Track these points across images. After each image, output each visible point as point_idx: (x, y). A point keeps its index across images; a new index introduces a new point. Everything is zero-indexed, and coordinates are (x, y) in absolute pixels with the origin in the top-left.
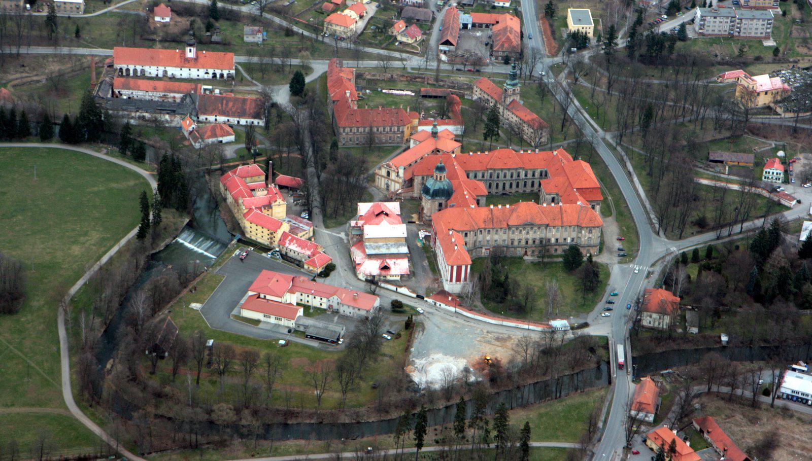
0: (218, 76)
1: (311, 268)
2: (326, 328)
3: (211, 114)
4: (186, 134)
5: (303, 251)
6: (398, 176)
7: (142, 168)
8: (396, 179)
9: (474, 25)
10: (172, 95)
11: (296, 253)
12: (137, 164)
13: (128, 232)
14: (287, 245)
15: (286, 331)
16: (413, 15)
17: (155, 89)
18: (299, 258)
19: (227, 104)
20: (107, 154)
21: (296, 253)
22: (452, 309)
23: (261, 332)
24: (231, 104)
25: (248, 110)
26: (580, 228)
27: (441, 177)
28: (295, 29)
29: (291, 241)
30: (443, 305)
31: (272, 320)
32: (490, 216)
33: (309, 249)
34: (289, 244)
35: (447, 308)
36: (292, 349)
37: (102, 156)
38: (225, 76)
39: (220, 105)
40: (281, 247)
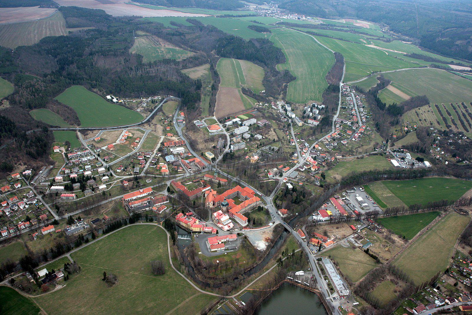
3: (157, 204)
15: (224, 250)
17: (139, 202)
20: (143, 223)
22: (249, 230)
28: (156, 176)
29: (205, 228)
30: (247, 230)
31: (219, 249)
37: (142, 224)
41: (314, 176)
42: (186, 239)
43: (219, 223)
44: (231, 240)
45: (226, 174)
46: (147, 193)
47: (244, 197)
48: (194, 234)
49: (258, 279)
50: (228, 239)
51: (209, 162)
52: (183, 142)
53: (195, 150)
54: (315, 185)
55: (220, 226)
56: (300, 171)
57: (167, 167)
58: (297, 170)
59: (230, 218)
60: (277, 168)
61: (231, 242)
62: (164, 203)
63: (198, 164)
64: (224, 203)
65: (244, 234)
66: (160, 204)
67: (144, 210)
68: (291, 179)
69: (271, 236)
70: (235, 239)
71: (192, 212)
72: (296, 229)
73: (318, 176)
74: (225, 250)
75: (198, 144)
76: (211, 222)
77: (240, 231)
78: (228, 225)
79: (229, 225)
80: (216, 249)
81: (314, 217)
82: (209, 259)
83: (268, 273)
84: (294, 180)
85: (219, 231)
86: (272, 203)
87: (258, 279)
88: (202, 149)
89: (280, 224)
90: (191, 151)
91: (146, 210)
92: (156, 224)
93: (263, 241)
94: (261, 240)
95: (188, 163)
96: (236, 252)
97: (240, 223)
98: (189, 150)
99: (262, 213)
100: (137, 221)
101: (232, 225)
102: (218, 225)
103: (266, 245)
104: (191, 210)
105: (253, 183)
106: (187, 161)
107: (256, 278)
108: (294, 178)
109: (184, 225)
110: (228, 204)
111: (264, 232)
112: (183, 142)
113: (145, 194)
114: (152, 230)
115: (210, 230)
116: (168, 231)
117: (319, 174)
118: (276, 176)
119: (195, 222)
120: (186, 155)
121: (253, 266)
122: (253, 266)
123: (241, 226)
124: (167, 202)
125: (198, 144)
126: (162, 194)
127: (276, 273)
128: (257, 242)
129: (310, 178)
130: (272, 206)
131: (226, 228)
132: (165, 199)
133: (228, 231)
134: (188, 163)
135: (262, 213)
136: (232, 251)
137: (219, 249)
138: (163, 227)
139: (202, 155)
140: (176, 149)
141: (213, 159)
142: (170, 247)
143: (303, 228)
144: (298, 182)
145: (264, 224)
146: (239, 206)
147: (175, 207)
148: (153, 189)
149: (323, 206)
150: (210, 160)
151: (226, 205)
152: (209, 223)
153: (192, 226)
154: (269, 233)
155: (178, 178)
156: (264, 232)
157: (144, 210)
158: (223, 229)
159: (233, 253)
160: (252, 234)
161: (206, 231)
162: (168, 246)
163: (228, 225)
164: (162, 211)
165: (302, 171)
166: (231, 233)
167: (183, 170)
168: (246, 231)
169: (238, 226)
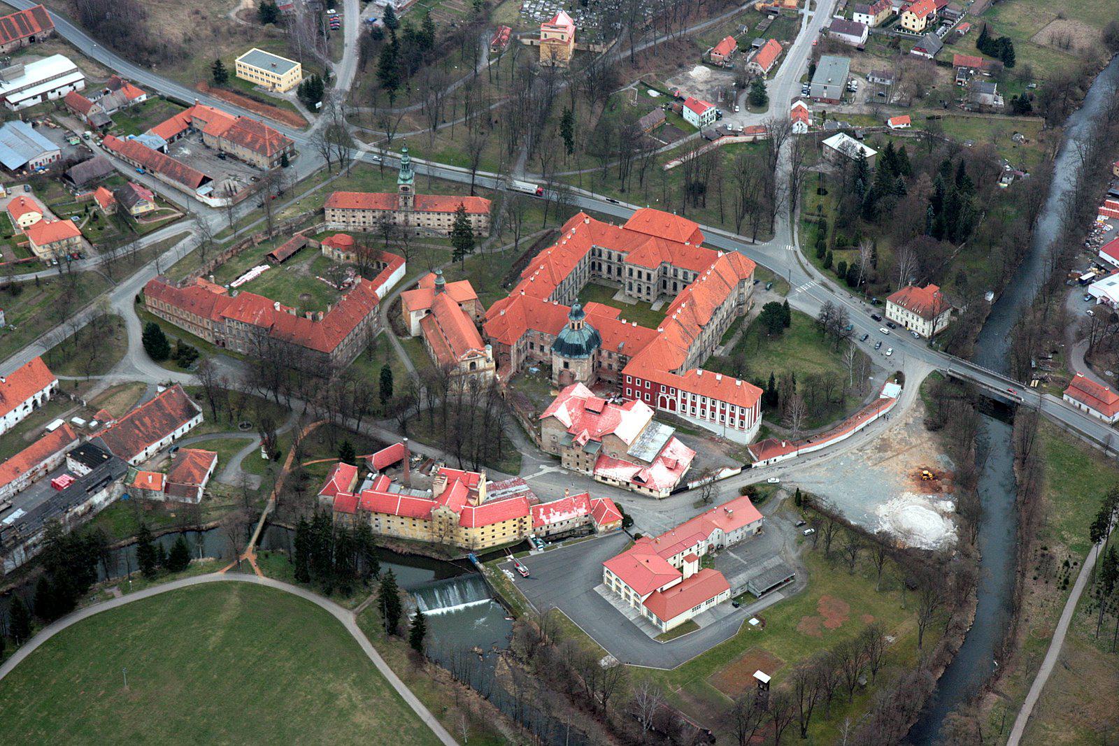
0: (39, 402)
1: (610, 525)
2: (767, 571)
3: (138, 452)
4: (161, 497)
5: (574, 514)
6: (488, 361)
7: (195, 575)
8: (487, 366)
9: (171, 140)
10: (42, 464)
11: (565, 523)
12: (182, 574)
13: (364, 654)
14: (546, 522)
15: (730, 609)
16: (89, 175)
17: (17, 472)
18: (569, 527)
19: (143, 424)
20: (125, 591)
21: (565, 523)
22: (794, 454)
23: (710, 633)
24: (147, 420)
25: (173, 413)
26: (88, 381)
27: (579, 324)
28: (19, 278)
29: (547, 512)
30: (779, 458)
31: (704, 607)
32: (682, 329)
33: (580, 507)
34: (548, 518)
35: (786, 457)
36: (778, 618)
37: (120, 600)
38: (48, 395)
39: (137, 431)
40: (538, 529)
41: (941, 58)
42: (461, 607)
43: (601, 459)
44: (734, 537)
45: (458, 173)
46: (30, 402)
47: (654, 275)
48: (498, 562)
49: (1027, 709)
50: (714, 539)
51: (290, 114)
52: (33, 21)
53: (145, 56)
54: (981, 109)
55: (623, 474)
56: (846, 49)
57: (43, 207)
58: (828, 45)
59: (660, 418)
60: (704, 63)
61: (735, 547)
62: (178, 433)
63: (235, 139)
64: (574, 338)
65: (777, 487)
66: (156, 445)
67: (80, 509)
68: (831, 110)
69: (937, 456)
70: (754, 527)
71: (397, 444)
72: (1042, 380)
73: (966, 54)
74: (736, 602)
75: (144, 16)
76: (546, 469)
77: (746, 474)
78: (665, 460)
79: (666, 454)
80: (688, 615)
81: (1093, 290)
82: (683, 683)
83: (1063, 663)
84: (846, 109)
85: (631, 507)
86: (811, 268)
87: (1027, 709)
88: (188, 40)
89: (934, 374)
90: (125, 70)
91: (91, 508)
92: (219, 576)
93: (907, 495)
94: (895, 493)
95: (161, 150)
96: (808, 599)
97: (716, 428)
98: (101, 65)
99: (796, 340)
100: (85, 591)
101: (682, 453)
102: (601, 472)
103: (944, 514)
104: (386, 435)
105: (633, 180)
106: (152, 139)
107: (1015, 708)
108: (843, 100)
109: (416, 532)
110: (595, 339)
111: (884, 446)
112: (33, 21)
113: (20, 408)
114: (223, 617)
115: (576, 516)
116: (328, 593)
117: (962, 43)
118: (732, 111)
119: (473, 494)
120: (113, 101)
121: (948, 647)
122: (948, 647)
123: (731, 443)
124: (193, 423)
125: (144, 16)
126: (124, 386)
127: (1101, 647)
128: (882, 510)
129: (931, 79)
130: (824, 285)
131: (663, 479)
132: (174, 409)
133: (679, 490)
134: (161, 150)
135: (796, 340)
136: (777, 597)
137: (704, 607)
138: (283, 578)
139: (221, 78)
140: (20, 73)
141: (312, 92)
142: (408, 682)
143: (1081, 372)
144: (875, 117)
145: (850, 403)
146: (668, 331)
147: (853, 458)
148: (54, 361)
149: (1101, 219)
150: (288, 104)
151: (589, 346)
152: (537, 476)
153: (465, 521)
154: (914, 441)
155: (170, 257)
156: (884, 446)
157: (80, 509)
158: (644, 491)
159: (791, 609)
160: (821, 473)
161: (558, 529)
162: (385, 682)
163: (665, 460)
164: (203, 484)
165: (860, 49)
166: (706, 501)
167: (159, 199)
168: (780, 466)
169: (717, 452)
